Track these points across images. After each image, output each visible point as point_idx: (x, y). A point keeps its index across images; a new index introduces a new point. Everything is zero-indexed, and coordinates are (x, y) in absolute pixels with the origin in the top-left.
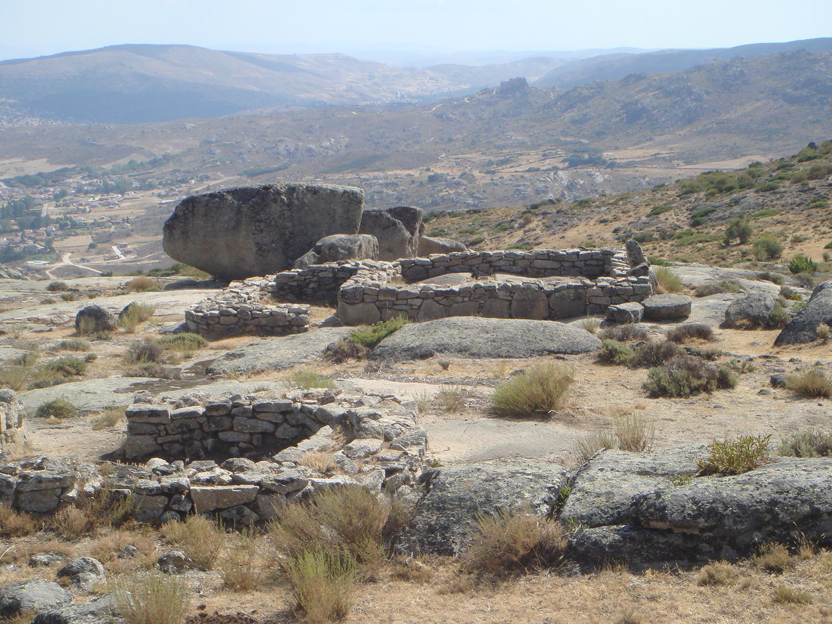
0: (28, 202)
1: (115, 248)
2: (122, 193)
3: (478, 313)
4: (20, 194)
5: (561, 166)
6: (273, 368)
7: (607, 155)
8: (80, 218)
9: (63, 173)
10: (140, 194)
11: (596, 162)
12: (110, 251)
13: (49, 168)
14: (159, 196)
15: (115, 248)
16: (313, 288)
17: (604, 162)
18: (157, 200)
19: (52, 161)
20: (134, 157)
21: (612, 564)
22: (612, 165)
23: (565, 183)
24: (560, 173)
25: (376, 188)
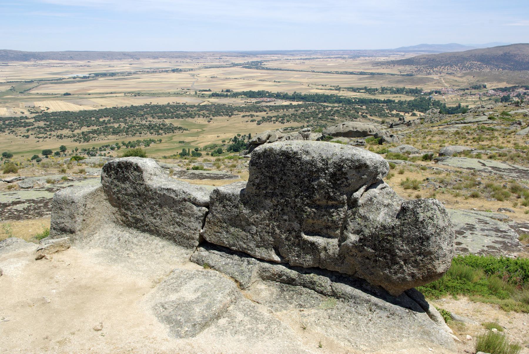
9: (515, 87)
13: (508, 86)
19: (508, 82)
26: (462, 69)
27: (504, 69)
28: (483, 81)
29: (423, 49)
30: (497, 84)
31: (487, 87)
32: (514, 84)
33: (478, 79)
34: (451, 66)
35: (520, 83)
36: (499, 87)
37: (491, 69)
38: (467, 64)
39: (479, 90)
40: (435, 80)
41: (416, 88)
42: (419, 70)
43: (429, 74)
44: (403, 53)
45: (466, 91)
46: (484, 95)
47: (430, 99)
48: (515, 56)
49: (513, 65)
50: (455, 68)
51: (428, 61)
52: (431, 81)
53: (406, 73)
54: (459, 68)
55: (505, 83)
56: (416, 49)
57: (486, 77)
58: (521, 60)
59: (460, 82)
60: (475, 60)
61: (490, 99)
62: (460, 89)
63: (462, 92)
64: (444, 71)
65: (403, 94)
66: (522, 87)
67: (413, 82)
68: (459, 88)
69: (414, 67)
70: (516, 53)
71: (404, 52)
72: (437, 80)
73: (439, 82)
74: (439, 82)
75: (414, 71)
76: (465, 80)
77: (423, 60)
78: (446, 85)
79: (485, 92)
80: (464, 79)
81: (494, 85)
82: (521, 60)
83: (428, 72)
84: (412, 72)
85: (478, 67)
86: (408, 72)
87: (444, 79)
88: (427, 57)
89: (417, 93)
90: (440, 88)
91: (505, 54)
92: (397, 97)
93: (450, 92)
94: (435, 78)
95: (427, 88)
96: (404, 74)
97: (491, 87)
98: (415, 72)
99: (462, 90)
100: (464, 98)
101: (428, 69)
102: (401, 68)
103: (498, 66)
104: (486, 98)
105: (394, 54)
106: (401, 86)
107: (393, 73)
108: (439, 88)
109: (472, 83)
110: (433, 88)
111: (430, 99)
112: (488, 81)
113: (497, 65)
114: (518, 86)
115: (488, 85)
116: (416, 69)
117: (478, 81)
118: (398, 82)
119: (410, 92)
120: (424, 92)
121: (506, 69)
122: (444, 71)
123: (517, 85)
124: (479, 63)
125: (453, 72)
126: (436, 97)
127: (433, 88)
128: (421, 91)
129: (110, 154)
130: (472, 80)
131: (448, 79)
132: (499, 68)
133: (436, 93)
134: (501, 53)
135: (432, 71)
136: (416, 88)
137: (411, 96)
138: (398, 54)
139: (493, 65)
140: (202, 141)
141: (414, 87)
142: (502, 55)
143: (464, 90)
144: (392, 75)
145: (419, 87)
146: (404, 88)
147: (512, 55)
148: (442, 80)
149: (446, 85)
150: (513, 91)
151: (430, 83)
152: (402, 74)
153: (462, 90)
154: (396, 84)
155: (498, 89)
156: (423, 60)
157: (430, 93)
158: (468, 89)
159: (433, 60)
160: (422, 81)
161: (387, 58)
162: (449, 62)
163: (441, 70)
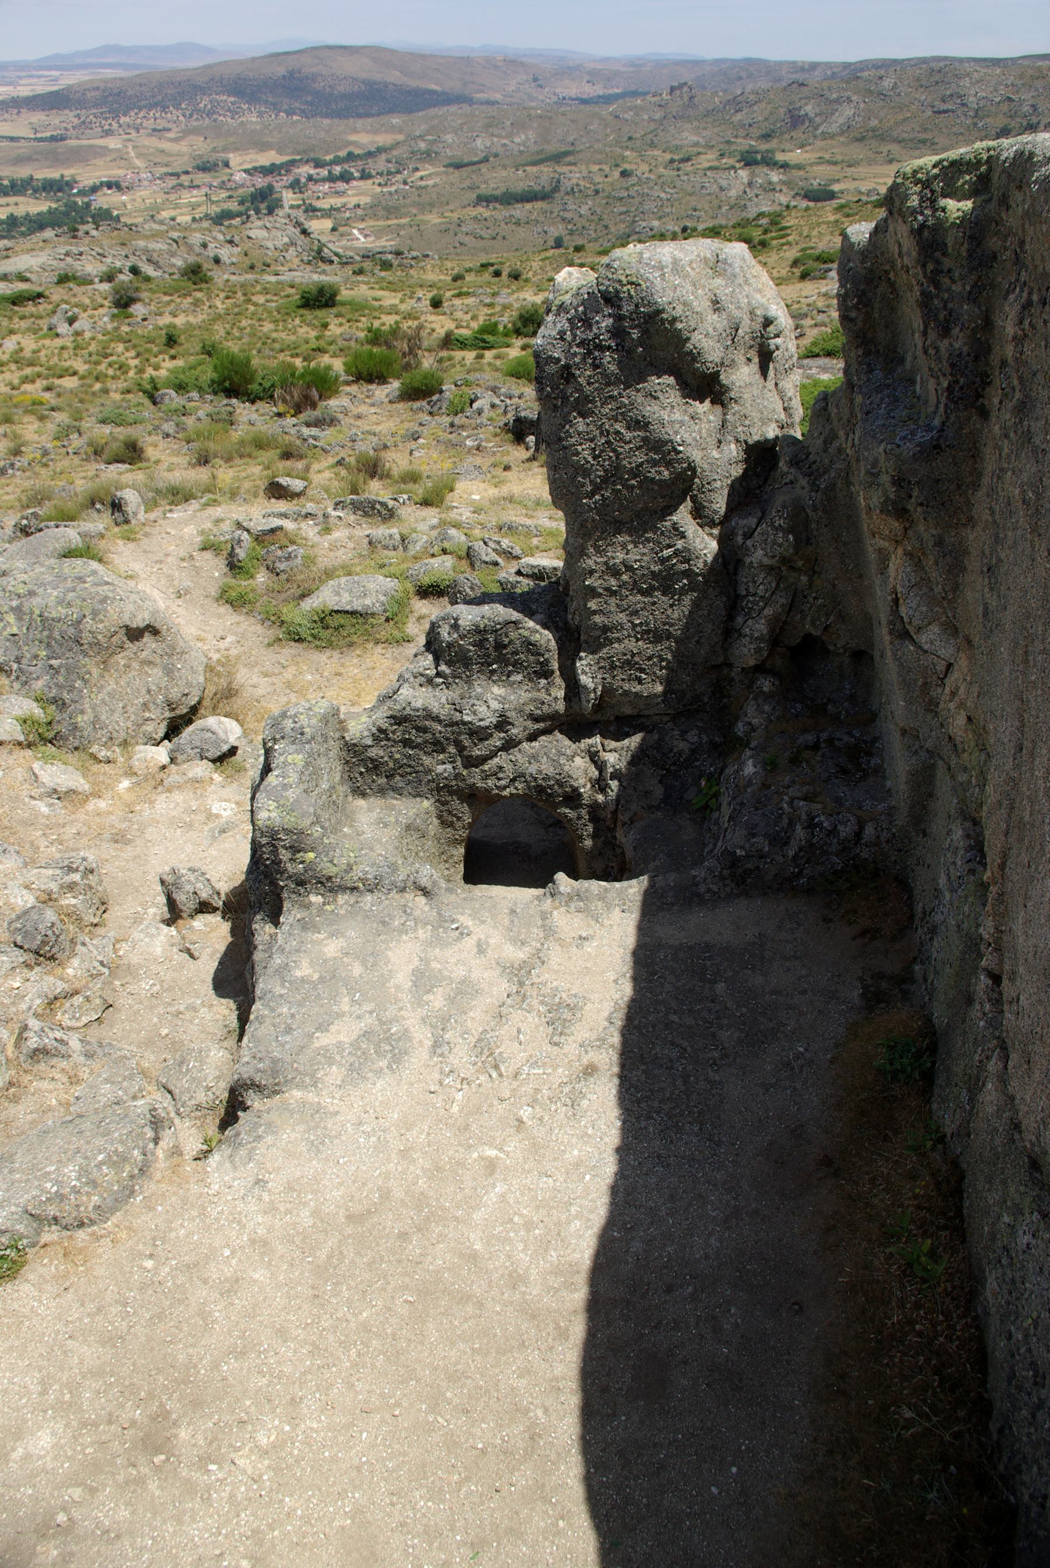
0: (270, 188)
1: (355, 231)
2: (347, 182)
3: (903, 884)
4: (260, 182)
5: (738, 165)
6: (237, 703)
7: (780, 157)
8: (319, 204)
9: (293, 163)
10: (361, 183)
11: (770, 163)
12: (350, 234)
13: (279, 159)
14: (380, 185)
15: (355, 231)
16: (37, 814)
17: (775, 164)
18: (378, 189)
19: (280, 152)
20: (351, 149)
21: (694, 359)
22: (785, 166)
23: (746, 181)
24: (740, 172)
25: (575, 181)
26: (191, 115)
27: (290, 113)
28: (225, 149)
29: (111, 60)
30: (254, 156)
31: (231, 164)
32: (292, 153)
33: (215, 144)
34: (164, 109)
35: (305, 152)
36: (257, 164)
37: (260, 115)
38: (204, 102)
39: (213, 174)
40: (111, 151)
41: (62, 176)
42: (84, 122)
43: (108, 133)
44: (55, 73)
45: (183, 178)
46: (222, 186)
47: (88, 205)
48: (314, 78)
49: (311, 104)
50: (174, 114)
51: (106, 97)
52: (101, 155)
53: (48, 134)
54: (184, 116)
55: (273, 153)
56: (93, 60)
57: (232, 140)
58: (328, 89)
59: (172, 155)
60: (222, 93)
61: (230, 197)
62: (166, 174)
63: (172, 182)
64: (145, 123)
65: (25, 195)
66: (307, 161)
67: (55, 159)
68: (169, 170)
69: (72, 114)
70: (314, 70)
71: (57, 68)
72: (118, 150)
73: (121, 157)
74: (121, 157)
75: (69, 126)
76: (185, 149)
77: (93, 94)
78: (138, 163)
79: (225, 178)
80: (183, 147)
81: (248, 158)
82: (328, 89)
83: (107, 127)
84: (66, 129)
85: (229, 110)
86: (55, 129)
87: (134, 147)
88: (102, 85)
89: (60, 190)
90: (121, 172)
91: (291, 75)
92: (8, 205)
93: (145, 183)
94: (112, 146)
95: (86, 176)
96: (44, 135)
97: (241, 164)
98: (74, 128)
99: (172, 175)
100: (172, 197)
101: (106, 119)
102: (38, 117)
103: (276, 107)
104: (224, 194)
105: (31, 77)
106: (23, 172)
107: (15, 135)
108: (116, 173)
109: (200, 156)
110: (105, 173)
111: (88, 205)
112: (236, 149)
113: (274, 105)
114: (301, 160)
115: (234, 159)
116: (76, 121)
117: (214, 150)
118: (19, 161)
119: (44, 189)
120: (81, 186)
121: (294, 113)
122: (145, 123)
123: (298, 157)
124: (232, 99)
125: (170, 126)
126: (104, 200)
127: (105, 173)
128: (70, 185)
129: (451, 232)
130: (200, 146)
131: (144, 147)
132: (280, 111)
133: (110, 187)
134: (281, 71)
135: (115, 125)
136: (62, 176)
137: (46, 198)
138: (39, 77)
139: (266, 102)
140: (501, 212)
141: (54, 174)
142: (284, 77)
143: (177, 175)
144: (12, 139)
145: (68, 173)
146: (31, 178)
147: (307, 78)
148: (130, 149)
149: (138, 163)
150: (288, 171)
151: (99, 162)
152: (39, 135)
153: (172, 175)
154: (12, 168)
155: (255, 169)
156: (93, 94)
157: (94, 189)
158: (187, 173)
159: (119, 94)
160: (80, 156)
161: (10, 88)
162: (160, 98)
163: (139, 121)
